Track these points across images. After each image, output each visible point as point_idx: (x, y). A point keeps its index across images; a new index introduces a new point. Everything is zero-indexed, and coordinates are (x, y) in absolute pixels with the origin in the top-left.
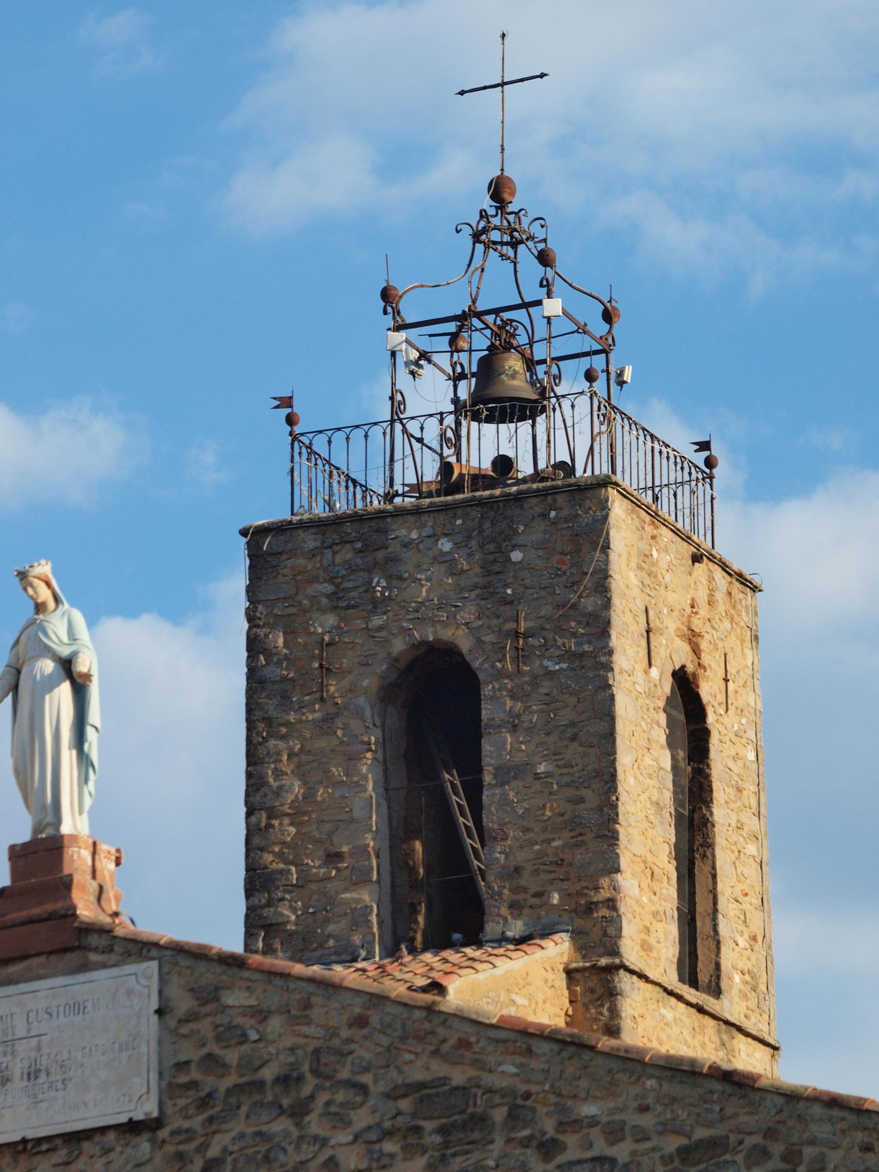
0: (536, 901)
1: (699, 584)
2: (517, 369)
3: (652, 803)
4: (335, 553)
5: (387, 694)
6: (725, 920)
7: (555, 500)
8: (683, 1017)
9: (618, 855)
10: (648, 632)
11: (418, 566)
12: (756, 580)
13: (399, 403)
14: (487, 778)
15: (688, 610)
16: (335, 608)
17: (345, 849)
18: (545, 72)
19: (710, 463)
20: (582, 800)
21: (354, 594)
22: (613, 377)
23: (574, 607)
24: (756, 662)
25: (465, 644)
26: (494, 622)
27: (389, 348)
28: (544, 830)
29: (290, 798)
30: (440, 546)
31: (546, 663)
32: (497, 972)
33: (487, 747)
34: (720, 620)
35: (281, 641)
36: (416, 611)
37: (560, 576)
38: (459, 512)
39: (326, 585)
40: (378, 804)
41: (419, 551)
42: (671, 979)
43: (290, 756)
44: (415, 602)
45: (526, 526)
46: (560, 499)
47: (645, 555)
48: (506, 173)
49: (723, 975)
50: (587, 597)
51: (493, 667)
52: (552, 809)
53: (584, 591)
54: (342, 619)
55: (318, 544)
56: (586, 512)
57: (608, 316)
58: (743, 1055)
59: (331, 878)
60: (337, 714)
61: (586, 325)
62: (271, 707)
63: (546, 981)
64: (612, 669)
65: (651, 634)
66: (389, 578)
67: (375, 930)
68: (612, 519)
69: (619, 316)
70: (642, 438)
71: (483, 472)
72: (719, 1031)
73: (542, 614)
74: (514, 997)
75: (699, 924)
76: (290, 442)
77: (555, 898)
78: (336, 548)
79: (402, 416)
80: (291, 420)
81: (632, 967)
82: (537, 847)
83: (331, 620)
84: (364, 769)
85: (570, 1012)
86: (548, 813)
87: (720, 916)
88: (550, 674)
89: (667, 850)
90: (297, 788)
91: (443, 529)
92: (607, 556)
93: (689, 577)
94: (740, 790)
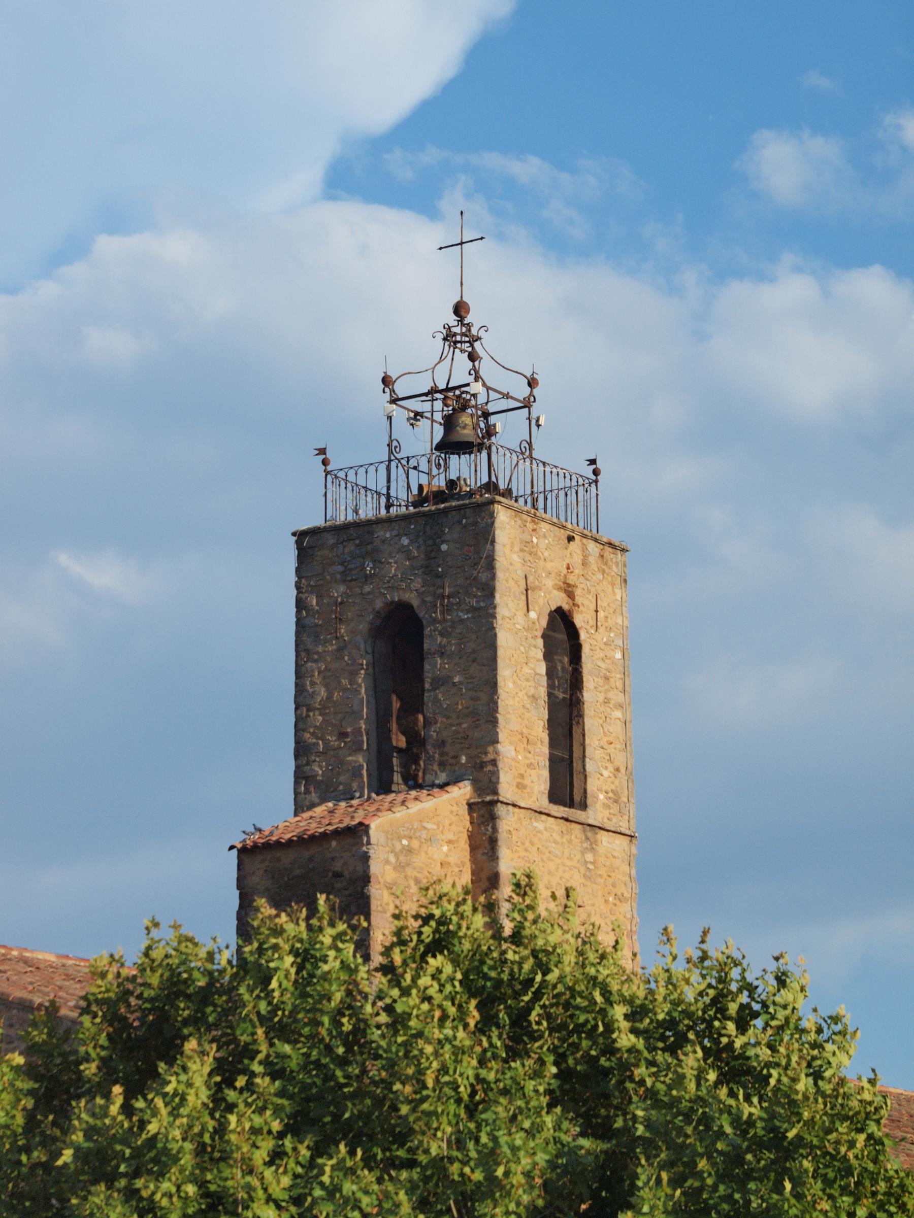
0: (453, 761)
3: (529, 697)
4: (345, 547)
5: (376, 633)
6: (591, 763)
7: (465, 512)
8: (553, 826)
9: (497, 733)
10: (527, 590)
13: (396, 447)
14: (427, 686)
15: (565, 571)
17: (349, 730)
20: (478, 699)
22: (533, 422)
24: (624, 596)
25: (415, 603)
26: (432, 589)
28: (458, 717)
29: (319, 699)
31: (460, 614)
32: (411, 811)
33: (427, 667)
35: (314, 602)
36: (388, 582)
40: (368, 702)
41: (390, 545)
42: (543, 803)
43: (319, 673)
46: (469, 512)
47: (527, 542)
48: (464, 299)
49: (588, 796)
51: (431, 616)
52: (462, 704)
54: (348, 588)
57: (532, 383)
58: (605, 843)
59: (341, 748)
60: (345, 647)
62: (308, 641)
63: (452, 812)
64: (495, 618)
65: (529, 592)
66: (374, 562)
67: (365, 780)
68: (497, 524)
69: (537, 384)
70: (534, 466)
72: (584, 831)
74: (425, 824)
75: (575, 765)
77: (463, 759)
78: (345, 543)
79: (398, 456)
80: (325, 462)
81: (505, 801)
82: (454, 728)
83: (342, 588)
84: (360, 681)
85: (470, 829)
86: (460, 707)
87: (587, 760)
88: (462, 621)
89: (542, 723)
90: (323, 692)
94: (607, 679)
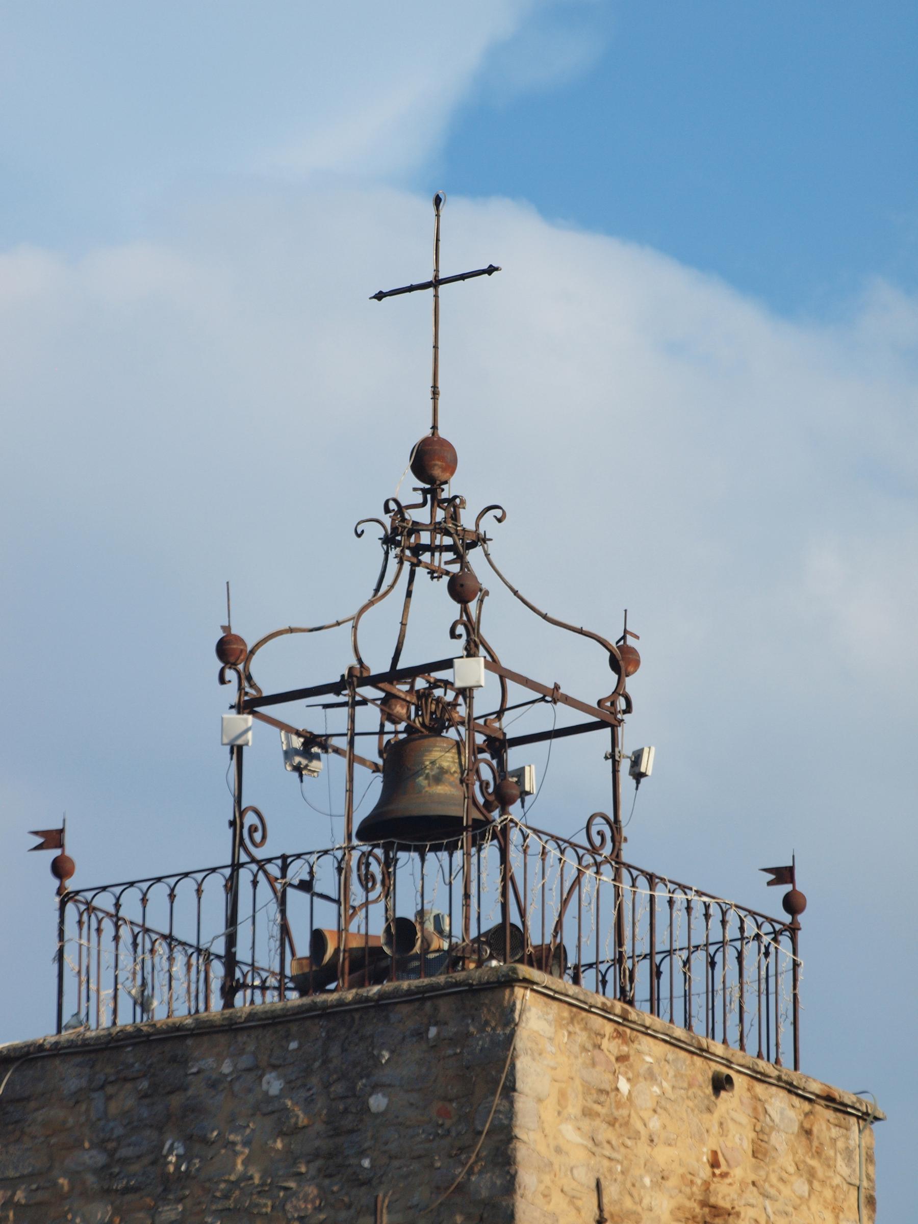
1: (731, 1125)
2: (445, 764)
4: (109, 1098)
7: (436, 1009)
11: (232, 1119)
12: (867, 1103)
13: (253, 829)
15: (705, 1172)
16: (108, 1191)
18: (495, 265)
19: (793, 904)
21: (135, 1168)
22: (625, 766)
23: (461, 1188)
27: (226, 741)
30: (265, 1086)
34: (781, 1180)
37: (442, 1137)
38: (294, 1028)
39: (94, 1152)
44: (225, 1181)
45: (392, 1052)
46: (445, 1007)
47: (601, 1091)
50: (481, 1172)
53: (476, 1162)
55: (84, 1083)
56: (482, 1030)
61: (557, 687)
66: (189, 1139)
68: (522, 1041)
69: (637, 663)
71: (372, 943)
73: (415, 1200)
76: (57, 906)
78: (110, 1090)
80: (61, 869)
91: (270, 1056)
92: (512, 1103)
93: (706, 1116)
